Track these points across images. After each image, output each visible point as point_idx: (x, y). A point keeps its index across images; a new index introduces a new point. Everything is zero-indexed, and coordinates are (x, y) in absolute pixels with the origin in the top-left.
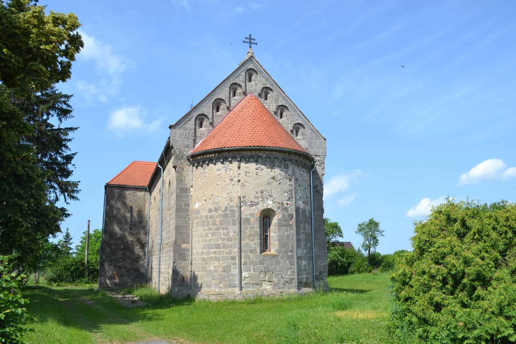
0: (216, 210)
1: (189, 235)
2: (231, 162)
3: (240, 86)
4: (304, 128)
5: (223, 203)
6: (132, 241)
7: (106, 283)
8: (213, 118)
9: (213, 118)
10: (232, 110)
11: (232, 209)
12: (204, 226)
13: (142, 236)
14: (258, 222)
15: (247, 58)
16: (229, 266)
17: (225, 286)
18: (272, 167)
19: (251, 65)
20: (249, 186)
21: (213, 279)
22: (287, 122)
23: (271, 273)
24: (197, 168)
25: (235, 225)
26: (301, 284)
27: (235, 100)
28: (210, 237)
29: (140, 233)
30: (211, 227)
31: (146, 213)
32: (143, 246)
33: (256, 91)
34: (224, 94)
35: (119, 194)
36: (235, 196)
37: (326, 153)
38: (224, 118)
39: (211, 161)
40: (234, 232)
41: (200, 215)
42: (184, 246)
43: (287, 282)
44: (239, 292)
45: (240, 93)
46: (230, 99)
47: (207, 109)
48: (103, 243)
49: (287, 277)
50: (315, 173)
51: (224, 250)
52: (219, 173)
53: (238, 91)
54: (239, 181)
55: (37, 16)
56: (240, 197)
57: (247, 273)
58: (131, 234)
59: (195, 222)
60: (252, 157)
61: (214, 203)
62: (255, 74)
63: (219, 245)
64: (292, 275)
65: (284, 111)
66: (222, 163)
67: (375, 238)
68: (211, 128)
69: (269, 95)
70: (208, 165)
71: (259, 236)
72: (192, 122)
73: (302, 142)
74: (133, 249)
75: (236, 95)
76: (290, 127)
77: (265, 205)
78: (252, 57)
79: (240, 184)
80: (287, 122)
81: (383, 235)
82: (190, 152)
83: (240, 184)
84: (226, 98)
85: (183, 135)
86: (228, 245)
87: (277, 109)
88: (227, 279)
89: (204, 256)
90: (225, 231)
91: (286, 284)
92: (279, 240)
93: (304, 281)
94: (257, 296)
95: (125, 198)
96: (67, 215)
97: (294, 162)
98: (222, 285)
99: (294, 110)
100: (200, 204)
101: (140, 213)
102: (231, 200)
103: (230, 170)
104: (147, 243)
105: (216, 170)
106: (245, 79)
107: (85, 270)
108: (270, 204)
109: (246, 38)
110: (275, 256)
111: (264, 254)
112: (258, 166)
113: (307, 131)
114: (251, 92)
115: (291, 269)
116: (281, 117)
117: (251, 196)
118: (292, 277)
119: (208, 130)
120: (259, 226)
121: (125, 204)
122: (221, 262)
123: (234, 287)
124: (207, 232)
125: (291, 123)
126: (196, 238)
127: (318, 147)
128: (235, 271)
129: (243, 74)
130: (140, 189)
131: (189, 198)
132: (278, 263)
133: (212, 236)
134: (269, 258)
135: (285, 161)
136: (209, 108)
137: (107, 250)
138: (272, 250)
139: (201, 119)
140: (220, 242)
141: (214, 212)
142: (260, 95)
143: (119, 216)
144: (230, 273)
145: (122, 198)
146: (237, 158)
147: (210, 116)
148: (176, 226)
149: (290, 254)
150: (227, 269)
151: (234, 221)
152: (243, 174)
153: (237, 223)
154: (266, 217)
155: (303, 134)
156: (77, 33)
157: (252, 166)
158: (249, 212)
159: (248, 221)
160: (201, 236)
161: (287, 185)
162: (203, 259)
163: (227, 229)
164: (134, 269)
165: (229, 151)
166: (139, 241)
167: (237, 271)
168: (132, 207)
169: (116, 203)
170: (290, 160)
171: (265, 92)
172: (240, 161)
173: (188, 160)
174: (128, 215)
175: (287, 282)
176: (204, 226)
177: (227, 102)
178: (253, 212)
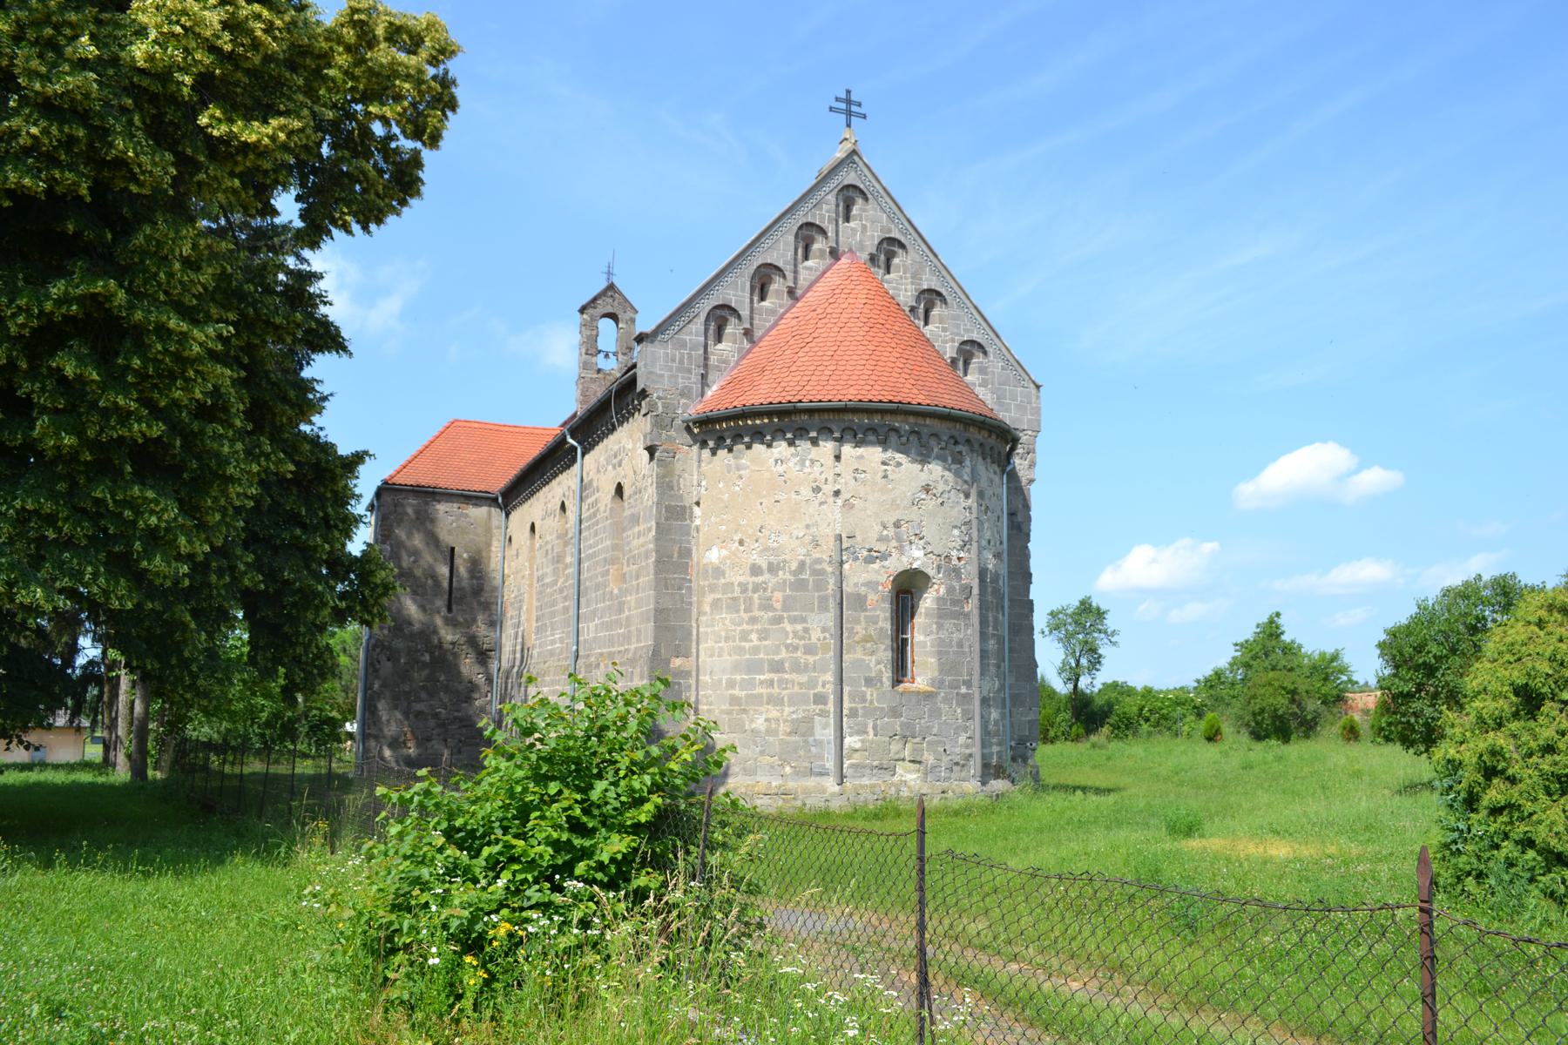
0: (773, 569)
1: (690, 634)
2: (815, 442)
3: (823, 232)
4: (985, 353)
5: (794, 550)
6: (453, 644)
7: (383, 758)
8: (752, 318)
9: (752, 318)
10: (803, 296)
11: (818, 567)
12: (738, 611)
13: (481, 629)
14: (887, 606)
15: (840, 155)
16: (808, 720)
17: (797, 773)
18: (924, 459)
19: (853, 174)
20: (865, 509)
21: (762, 753)
22: (943, 332)
23: (918, 740)
24: (714, 453)
25: (826, 610)
26: (990, 770)
27: (810, 269)
28: (756, 642)
29: (474, 620)
30: (756, 613)
31: (493, 566)
32: (483, 656)
33: (862, 248)
34: (781, 251)
35: (417, 512)
36: (827, 533)
37: (1039, 422)
38: (781, 318)
39: (758, 435)
40: (824, 630)
41: (723, 581)
42: (677, 662)
43: (957, 764)
44: (837, 789)
45: (822, 251)
46: (795, 266)
47: (737, 293)
48: (375, 646)
49: (957, 750)
50: (1013, 477)
51: (794, 676)
52: (780, 469)
53: (816, 246)
54: (837, 493)
55: (361, 21)
56: (839, 538)
57: (856, 738)
58: (451, 623)
59: (709, 598)
60: (872, 429)
61: (767, 549)
62: (860, 201)
63: (781, 662)
64: (967, 747)
65: (770, 281)
66: (791, 443)
67: (1093, 650)
68: (746, 345)
69: (896, 261)
70: (749, 447)
71: (888, 642)
72: (698, 325)
73: (983, 390)
74: (457, 666)
75: (811, 255)
76: (950, 351)
77: (904, 559)
78: (854, 152)
79: (840, 502)
80: (943, 332)
81: (1114, 644)
82: (694, 409)
83: (840, 502)
84: (786, 263)
85: (673, 360)
86: (806, 665)
87: (918, 299)
88: (802, 753)
89: (736, 692)
90: (799, 627)
91: (956, 768)
92: (940, 653)
93: (994, 761)
94: (884, 799)
95: (433, 521)
96: (1271, 630)
97: (976, 446)
98: (788, 769)
99: (961, 305)
100: (724, 552)
101: (477, 566)
102: (816, 544)
103: (813, 462)
104: (497, 647)
105: (773, 460)
106: (837, 213)
107: (298, 720)
108: (916, 557)
109: (837, 99)
110: (928, 696)
111: (901, 687)
112: (889, 454)
113: (994, 363)
114: (851, 250)
115: (966, 729)
116: (926, 323)
117: (870, 535)
118: (968, 751)
119: (740, 350)
120: (888, 614)
121: (433, 539)
122: (787, 710)
123: (821, 774)
124: (745, 626)
125: (953, 340)
126: (710, 643)
127: (1020, 408)
128: (825, 733)
129: (831, 198)
130: (477, 498)
131: (688, 534)
132: (935, 713)
133: (759, 639)
134: (914, 700)
135: (956, 443)
136: (743, 290)
137: (386, 667)
138: (918, 679)
139: (721, 316)
140: (784, 654)
141: (766, 576)
142: (873, 259)
143: (418, 572)
144: (811, 739)
145: (424, 521)
146: (831, 431)
147: (745, 313)
148: (656, 610)
149: (963, 690)
150: (802, 728)
151: (823, 601)
152: (847, 476)
153: (832, 604)
154: (906, 591)
155: (982, 370)
156: (446, 72)
157: (874, 454)
158: (864, 577)
159: (860, 601)
160: (727, 639)
161: (962, 507)
162: (735, 700)
163: (804, 620)
164: (461, 720)
165: (811, 412)
166: (472, 641)
167: (829, 734)
168: (453, 549)
169: (410, 535)
170: (968, 441)
171: (888, 249)
172: (840, 440)
173: (688, 429)
174: (444, 570)
175: (957, 764)
176: (738, 611)
177: (790, 275)
178: (874, 577)
